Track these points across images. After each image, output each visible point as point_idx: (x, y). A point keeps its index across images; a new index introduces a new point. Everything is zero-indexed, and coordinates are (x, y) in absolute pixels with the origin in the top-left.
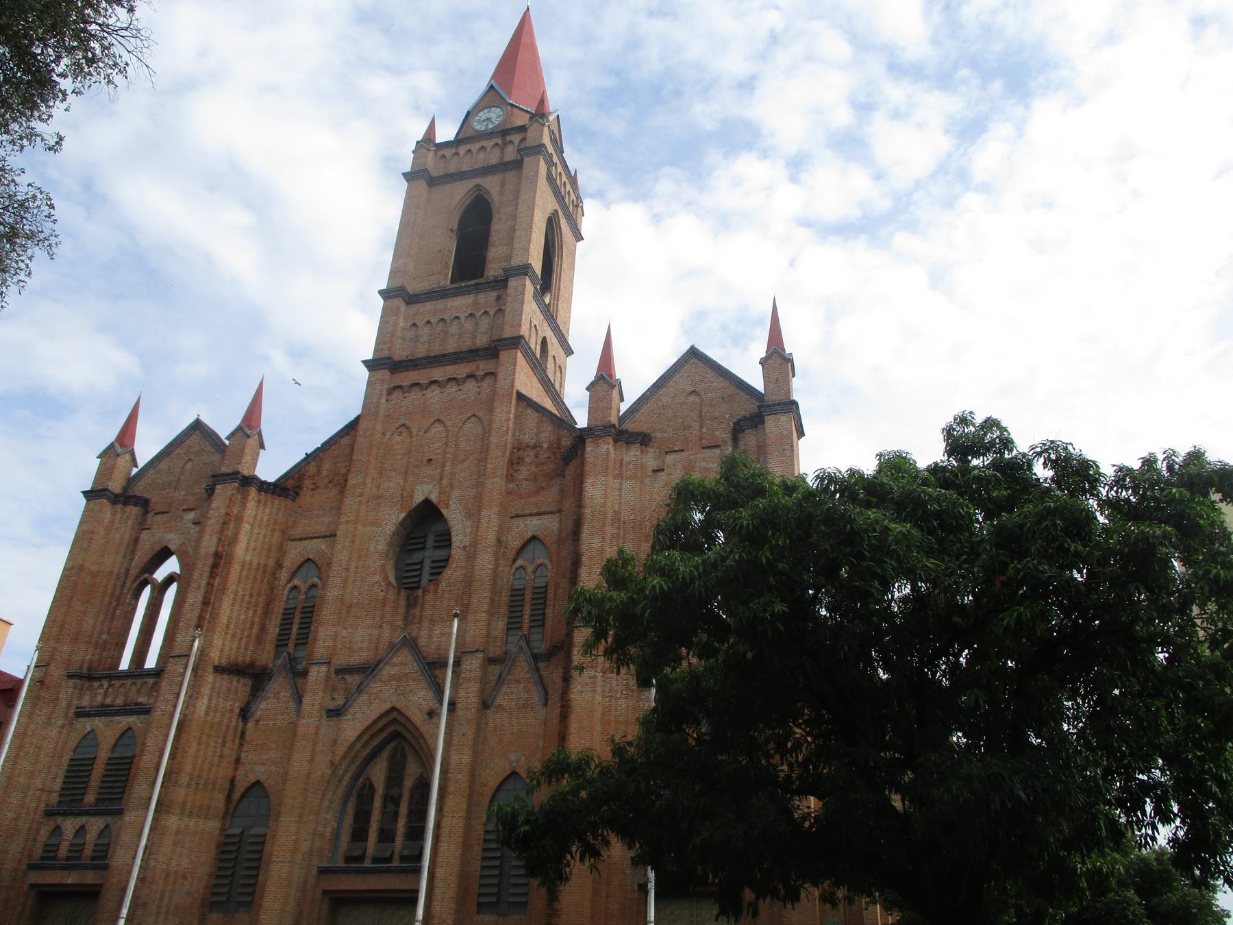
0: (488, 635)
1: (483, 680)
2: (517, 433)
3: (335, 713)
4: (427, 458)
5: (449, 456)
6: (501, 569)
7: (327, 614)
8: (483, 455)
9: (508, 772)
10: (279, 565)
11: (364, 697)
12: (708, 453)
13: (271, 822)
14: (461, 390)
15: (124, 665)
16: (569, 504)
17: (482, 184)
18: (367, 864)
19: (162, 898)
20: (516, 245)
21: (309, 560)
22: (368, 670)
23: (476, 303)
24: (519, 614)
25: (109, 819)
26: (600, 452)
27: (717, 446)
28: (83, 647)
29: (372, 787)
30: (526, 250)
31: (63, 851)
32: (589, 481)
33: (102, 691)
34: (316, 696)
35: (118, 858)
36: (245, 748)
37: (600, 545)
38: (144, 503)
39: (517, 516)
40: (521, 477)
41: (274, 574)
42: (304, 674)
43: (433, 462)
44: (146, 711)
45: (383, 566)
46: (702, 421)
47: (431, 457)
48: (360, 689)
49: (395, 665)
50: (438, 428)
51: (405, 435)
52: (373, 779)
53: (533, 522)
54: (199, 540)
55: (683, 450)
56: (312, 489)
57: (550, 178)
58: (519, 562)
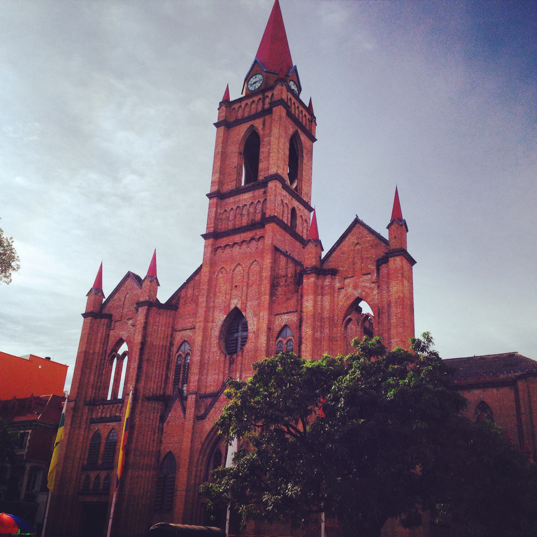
10: (172, 344)
11: (213, 409)
13: (177, 471)
14: (248, 247)
15: (109, 398)
23: (254, 196)
27: (369, 274)
29: (220, 452)
33: (100, 411)
39: (277, 314)
41: (170, 349)
43: (237, 287)
46: (362, 259)
48: (212, 405)
53: (285, 317)
56: (184, 304)
58: (280, 339)
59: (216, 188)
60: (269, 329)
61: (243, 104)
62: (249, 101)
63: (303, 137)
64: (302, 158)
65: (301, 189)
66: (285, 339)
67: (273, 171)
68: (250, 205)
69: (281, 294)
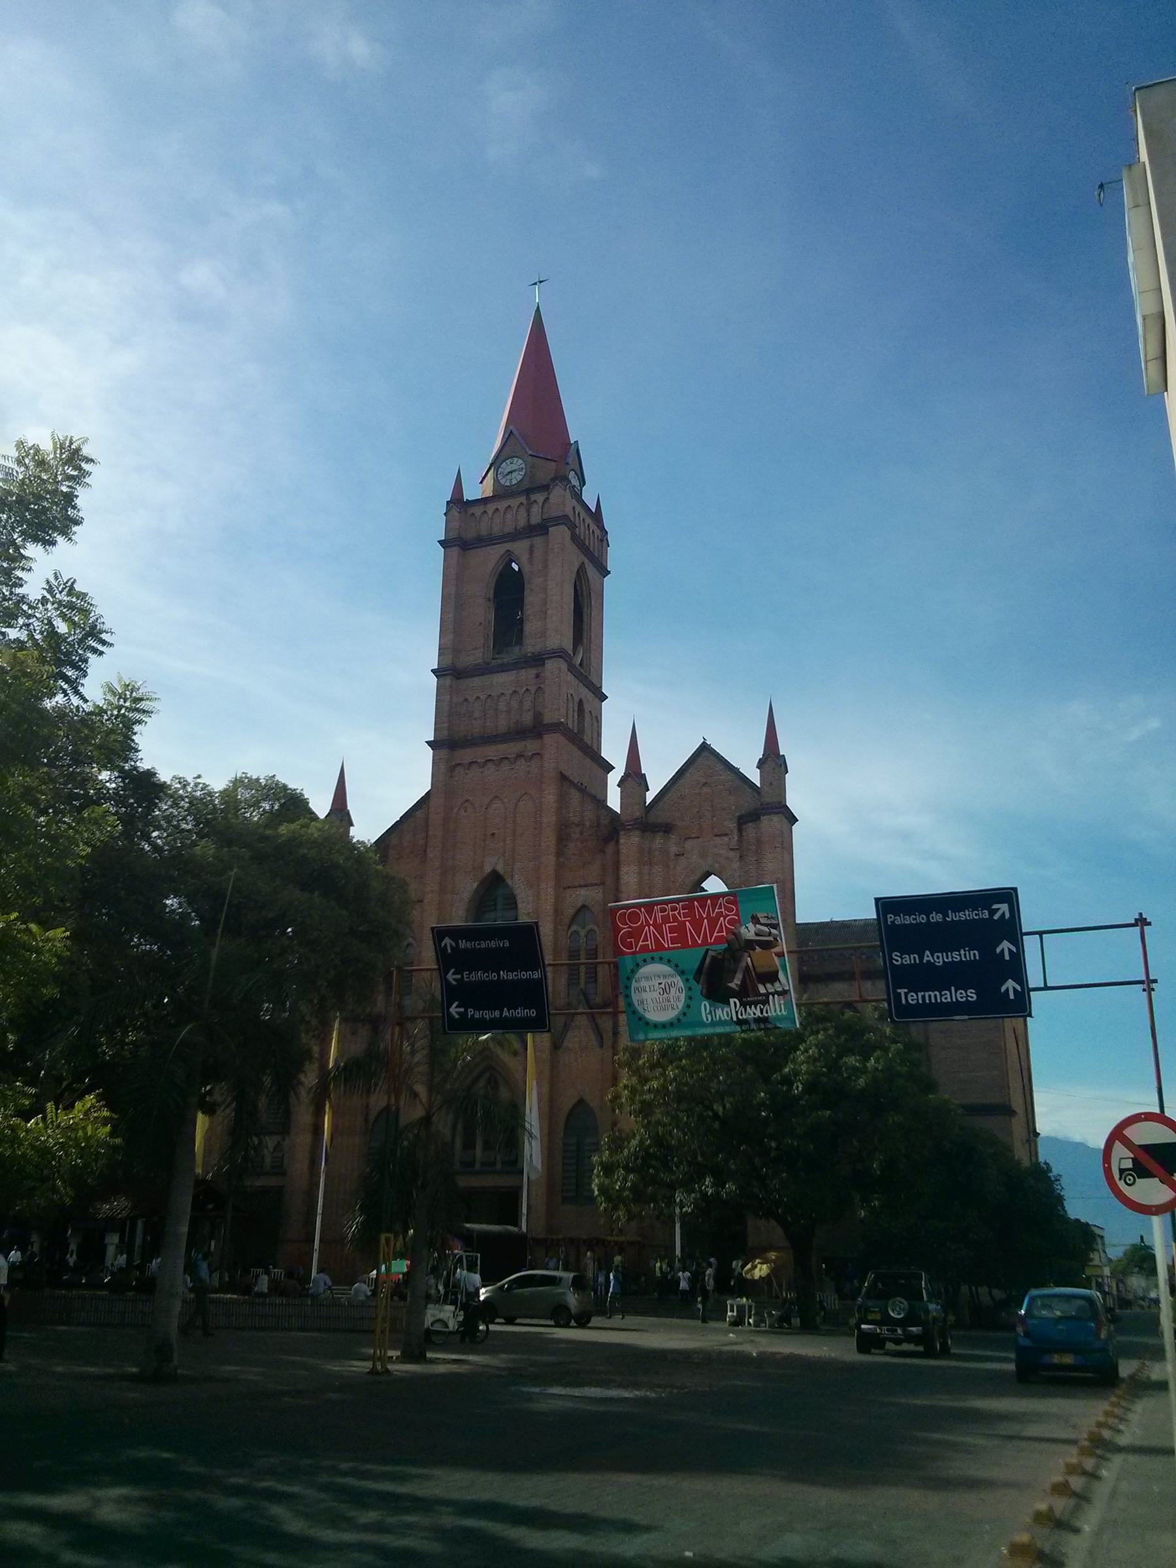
4: (490, 833)
26: (630, 842)
47: (494, 832)
55: (699, 838)
58: (574, 928)
59: (448, 660)
60: (557, 911)
61: (491, 508)
62: (502, 505)
63: (591, 571)
64: (589, 609)
65: (590, 665)
66: (584, 928)
67: (553, 642)
68: (511, 695)
69: (574, 854)
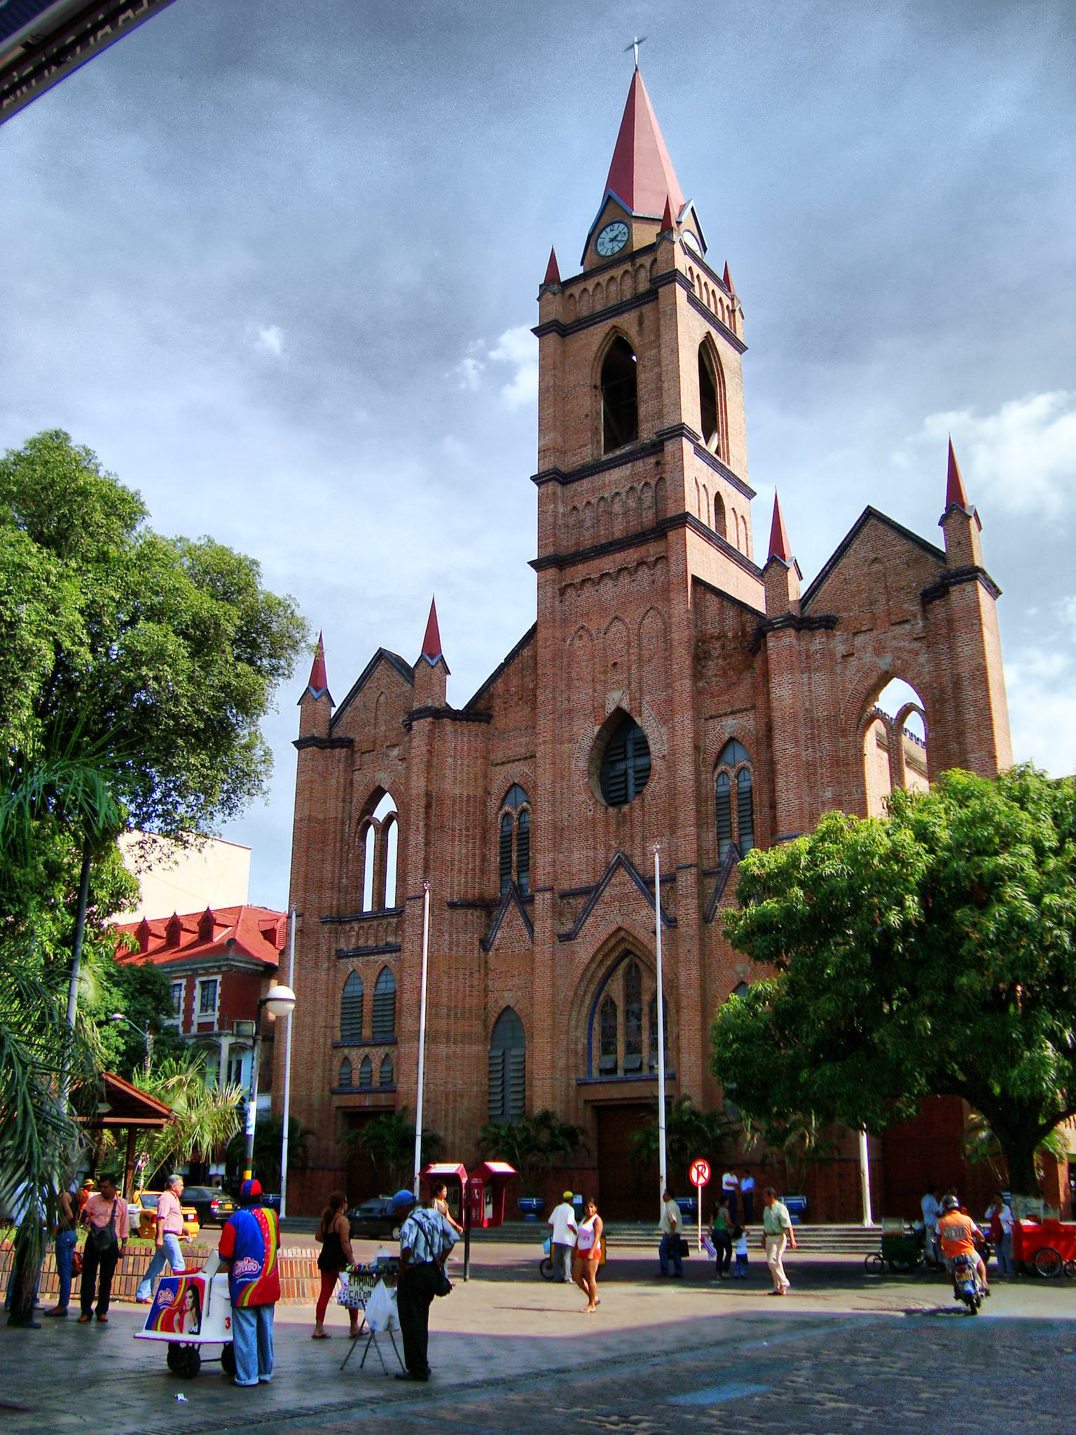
0: (699, 849)
1: (701, 895)
2: (699, 623)
3: (568, 937)
5: (633, 657)
6: (703, 776)
7: (542, 841)
8: (667, 654)
9: (736, 983)
11: (590, 920)
12: (898, 630)
15: (367, 907)
16: (760, 701)
17: (618, 325)
18: (620, 1073)
19: (446, 1116)
20: (666, 401)
21: (514, 784)
22: (591, 893)
24: (727, 817)
25: (387, 1049)
26: (780, 644)
27: (907, 621)
28: (328, 893)
29: (613, 1003)
30: (677, 405)
31: (356, 1081)
32: (775, 680)
34: (544, 926)
35: (402, 1086)
36: (490, 976)
37: (793, 750)
38: (348, 743)
39: (712, 717)
40: (710, 673)
41: (484, 803)
42: (531, 900)
44: (397, 949)
45: (587, 783)
46: (888, 593)
48: (587, 912)
49: (616, 886)
50: (618, 626)
51: (585, 638)
52: (612, 995)
54: (408, 778)
57: (693, 301)
58: (722, 767)
